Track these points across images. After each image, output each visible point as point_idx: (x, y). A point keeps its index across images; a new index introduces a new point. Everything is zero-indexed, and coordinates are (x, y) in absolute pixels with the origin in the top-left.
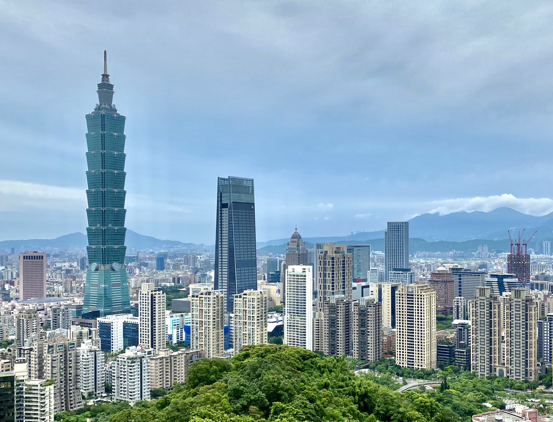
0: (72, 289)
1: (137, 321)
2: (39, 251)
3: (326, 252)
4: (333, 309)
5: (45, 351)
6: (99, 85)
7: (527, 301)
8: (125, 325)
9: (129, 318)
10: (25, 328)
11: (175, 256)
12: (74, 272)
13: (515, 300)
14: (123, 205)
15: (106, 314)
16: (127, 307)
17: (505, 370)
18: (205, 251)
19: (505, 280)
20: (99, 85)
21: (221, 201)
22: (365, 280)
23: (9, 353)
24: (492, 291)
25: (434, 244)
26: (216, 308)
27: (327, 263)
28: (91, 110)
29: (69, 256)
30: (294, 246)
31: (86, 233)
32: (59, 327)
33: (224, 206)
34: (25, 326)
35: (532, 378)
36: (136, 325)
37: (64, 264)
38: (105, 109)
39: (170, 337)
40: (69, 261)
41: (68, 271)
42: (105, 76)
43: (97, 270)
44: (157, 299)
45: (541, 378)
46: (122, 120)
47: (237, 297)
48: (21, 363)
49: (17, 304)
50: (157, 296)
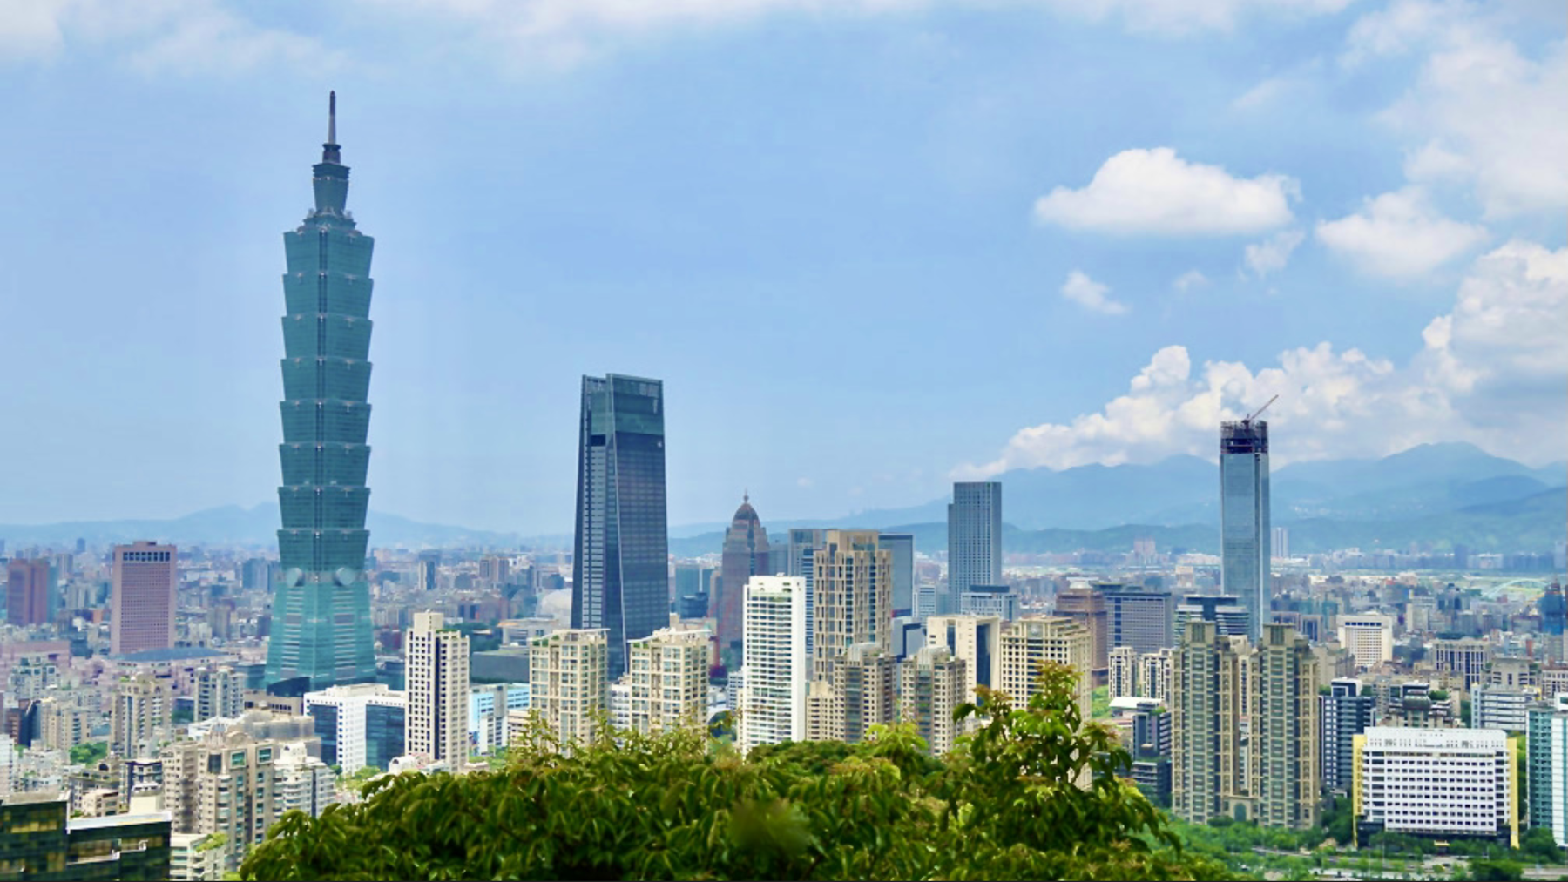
0: (230, 629)
1: (400, 699)
2: (159, 543)
3: (834, 547)
4: (854, 676)
5: (200, 768)
6: (317, 168)
7: (1297, 650)
8: (373, 713)
9: (382, 695)
10: (135, 717)
11: (457, 558)
12: (230, 591)
13: (1272, 648)
14: (363, 437)
15: (321, 686)
16: (368, 671)
17: (1248, 805)
18: (523, 549)
19: (1219, 609)
20: (317, 168)
21: (589, 429)
22: (908, 612)
23: (104, 773)
24: (1218, 631)
25: (1040, 535)
26: (590, 671)
27: (837, 572)
28: (295, 223)
29: (213, 558)
30: (742, 536)
31: (276, 498)
32: (214, 715)
33: (598, 440)
34: (135, 712)
35: (1310, 823)
36: (401, 711)
37: (204, 574)
38: (329, 218)
39: (474, 738)
40: (215, 568)
41: (217, 591)
42: (332, 150)
43: (300, 583)
44: (449, 649)
45: (1325, 822)
46: (366, 244)
47: (637, 646)
48: (145, 795)
49: (106, 663)
50: (449, 642)
